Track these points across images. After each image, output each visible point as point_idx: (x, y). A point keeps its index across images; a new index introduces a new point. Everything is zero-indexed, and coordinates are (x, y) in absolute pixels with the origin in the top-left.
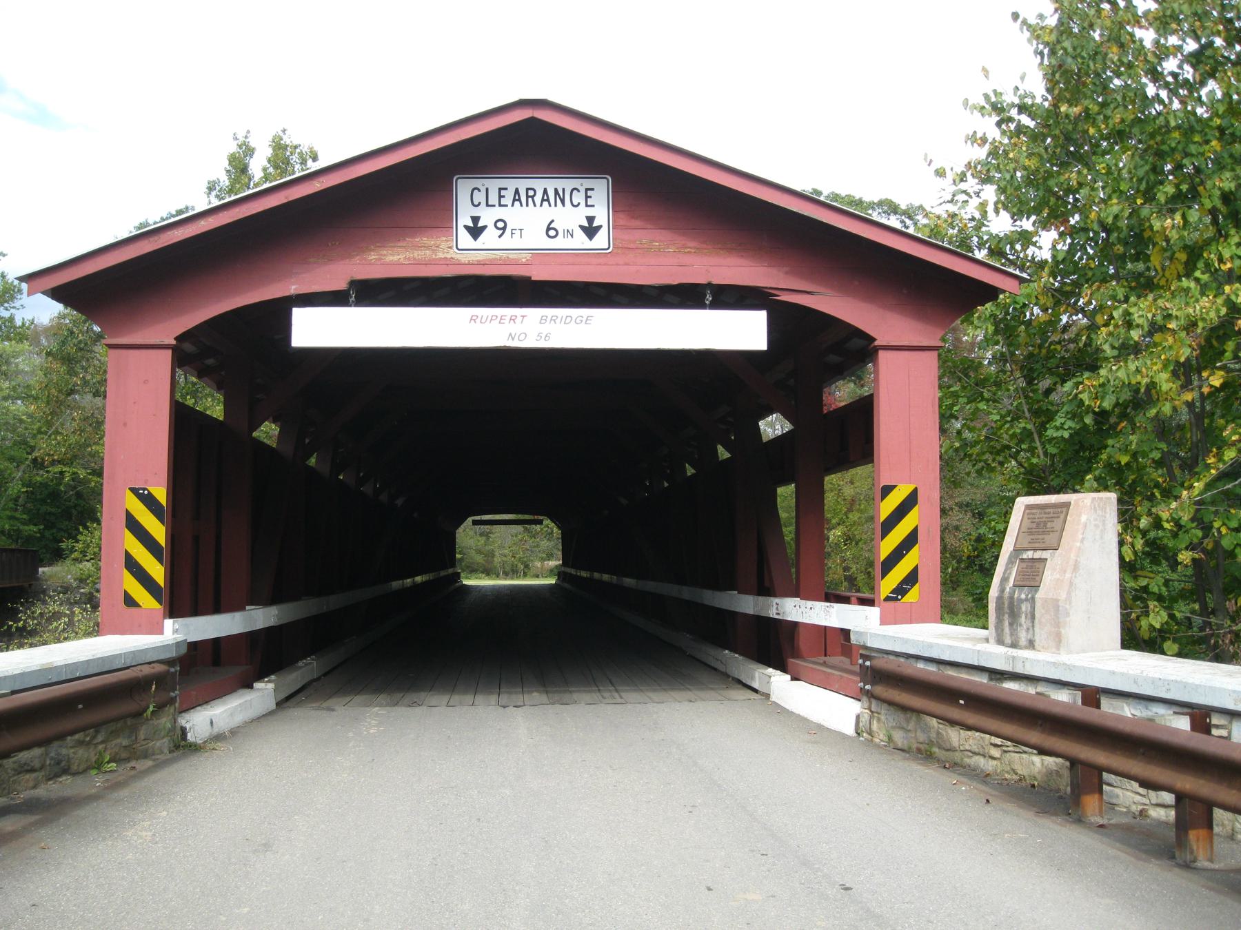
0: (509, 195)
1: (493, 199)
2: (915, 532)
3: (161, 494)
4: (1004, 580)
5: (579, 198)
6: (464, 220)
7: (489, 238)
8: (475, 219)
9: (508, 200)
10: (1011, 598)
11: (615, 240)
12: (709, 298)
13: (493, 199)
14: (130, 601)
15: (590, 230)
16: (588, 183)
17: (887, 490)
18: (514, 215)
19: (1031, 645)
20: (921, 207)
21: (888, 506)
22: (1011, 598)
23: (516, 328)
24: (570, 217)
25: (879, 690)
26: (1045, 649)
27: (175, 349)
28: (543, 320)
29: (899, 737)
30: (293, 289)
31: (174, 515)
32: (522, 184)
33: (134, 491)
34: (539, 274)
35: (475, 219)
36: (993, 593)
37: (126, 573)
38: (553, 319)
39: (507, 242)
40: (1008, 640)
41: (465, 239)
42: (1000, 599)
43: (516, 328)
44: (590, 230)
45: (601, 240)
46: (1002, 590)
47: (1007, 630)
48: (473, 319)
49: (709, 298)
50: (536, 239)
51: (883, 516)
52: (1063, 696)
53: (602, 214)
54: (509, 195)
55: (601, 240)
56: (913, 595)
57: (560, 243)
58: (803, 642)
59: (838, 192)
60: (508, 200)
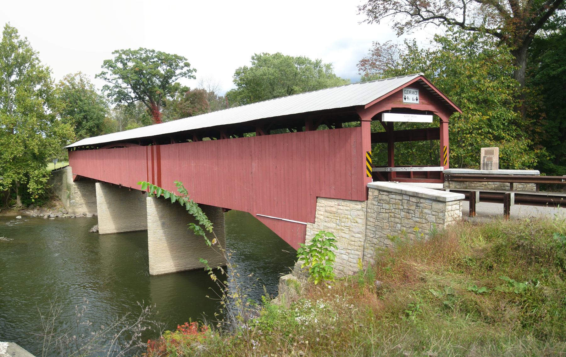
4: (484, 161)
6: (404, 97)
19: (491, 169)
20: (183, 57)
22: (487, 163)
25: (455, 179)
30: (385, 109)
34: (413, 108)
42: (484, 164)
44: (417, 100)
53: (418, 96)
55: (418, 102)
56: (446, 165)
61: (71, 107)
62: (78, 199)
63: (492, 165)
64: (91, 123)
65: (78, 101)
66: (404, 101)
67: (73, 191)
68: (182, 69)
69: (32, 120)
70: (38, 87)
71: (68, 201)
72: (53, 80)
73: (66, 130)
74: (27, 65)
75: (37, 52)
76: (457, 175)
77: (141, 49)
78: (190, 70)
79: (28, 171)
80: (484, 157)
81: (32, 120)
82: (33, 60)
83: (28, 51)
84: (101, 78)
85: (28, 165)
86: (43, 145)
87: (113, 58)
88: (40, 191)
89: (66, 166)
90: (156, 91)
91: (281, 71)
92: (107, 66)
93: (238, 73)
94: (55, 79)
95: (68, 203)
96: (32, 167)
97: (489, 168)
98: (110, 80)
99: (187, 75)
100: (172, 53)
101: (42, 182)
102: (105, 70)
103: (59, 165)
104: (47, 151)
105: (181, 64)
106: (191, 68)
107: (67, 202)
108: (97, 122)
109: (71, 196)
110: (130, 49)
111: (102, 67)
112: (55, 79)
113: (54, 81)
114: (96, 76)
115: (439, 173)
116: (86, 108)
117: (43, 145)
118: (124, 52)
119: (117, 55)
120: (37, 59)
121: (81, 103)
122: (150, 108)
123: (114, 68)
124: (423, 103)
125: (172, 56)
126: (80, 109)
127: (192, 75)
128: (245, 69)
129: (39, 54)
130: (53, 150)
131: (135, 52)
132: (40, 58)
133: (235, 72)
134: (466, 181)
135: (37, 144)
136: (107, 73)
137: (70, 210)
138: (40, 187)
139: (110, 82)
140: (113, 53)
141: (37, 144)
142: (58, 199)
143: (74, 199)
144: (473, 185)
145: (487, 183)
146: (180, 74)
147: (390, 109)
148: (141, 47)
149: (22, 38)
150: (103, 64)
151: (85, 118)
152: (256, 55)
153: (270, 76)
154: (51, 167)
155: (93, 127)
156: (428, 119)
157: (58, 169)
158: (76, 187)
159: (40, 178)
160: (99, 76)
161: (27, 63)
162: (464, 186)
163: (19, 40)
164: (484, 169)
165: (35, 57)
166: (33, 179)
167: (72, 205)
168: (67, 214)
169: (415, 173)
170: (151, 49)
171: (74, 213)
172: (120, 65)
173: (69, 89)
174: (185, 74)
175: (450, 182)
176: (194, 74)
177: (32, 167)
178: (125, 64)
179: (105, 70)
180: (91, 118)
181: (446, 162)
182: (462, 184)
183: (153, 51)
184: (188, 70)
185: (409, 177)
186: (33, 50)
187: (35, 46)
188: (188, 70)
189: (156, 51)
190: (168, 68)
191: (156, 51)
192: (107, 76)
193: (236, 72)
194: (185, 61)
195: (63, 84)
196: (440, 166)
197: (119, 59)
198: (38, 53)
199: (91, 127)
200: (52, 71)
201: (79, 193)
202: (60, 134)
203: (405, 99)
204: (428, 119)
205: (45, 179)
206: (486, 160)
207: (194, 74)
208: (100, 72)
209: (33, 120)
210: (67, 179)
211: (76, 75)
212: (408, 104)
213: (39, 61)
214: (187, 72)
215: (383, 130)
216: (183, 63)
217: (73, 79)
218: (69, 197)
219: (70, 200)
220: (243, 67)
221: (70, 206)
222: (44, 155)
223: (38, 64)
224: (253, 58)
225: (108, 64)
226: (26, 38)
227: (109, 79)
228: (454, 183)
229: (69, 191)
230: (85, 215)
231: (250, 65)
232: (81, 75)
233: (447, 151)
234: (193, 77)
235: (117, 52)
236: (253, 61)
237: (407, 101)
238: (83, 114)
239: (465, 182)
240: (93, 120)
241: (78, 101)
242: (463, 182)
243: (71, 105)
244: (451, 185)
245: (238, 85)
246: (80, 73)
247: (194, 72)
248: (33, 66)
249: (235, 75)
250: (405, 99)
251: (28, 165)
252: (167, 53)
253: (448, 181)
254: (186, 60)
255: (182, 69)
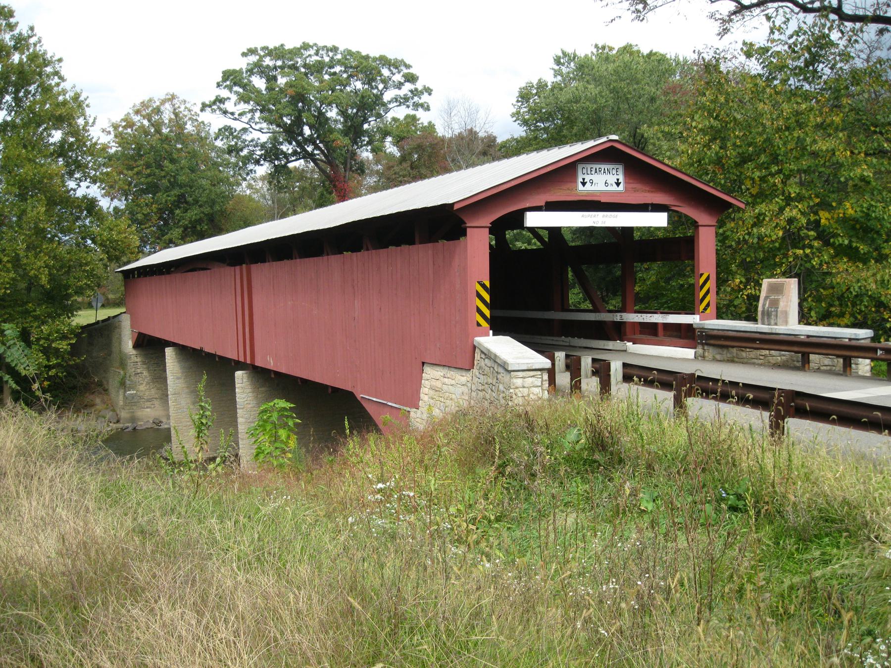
0: (594, 170)
1: (589, 172)
2: (709, 289)
3: (487, 284)
4: (764, 305)
5: (614, 172)
6: (580, 180)
7: (588, 187)
8: (584, 179)
9: (593, 172)
10: (768, 310)
11: (626, 188)
12: (650, 208)
13: (589, 172)
14: (479, 325)
15: (618, 184)
16: (617, 166)
17: (702, 275)
18: (596, 178)
19: (776, 324)
20: (402, 61)
21: (702, 281)
22: (768, 310)
23: (595, 219)
24: (612, 179)
25: (712, 342)
26: (782, 325)
27: (490, 228)
28: (603, 216)
29: (718, 357)
30: (528, 205)
31: (491, 291)
32: (598, 166)
33: (479, 282)
34: (603, 200)
35: (584, 179)
36: (760, 309)
37: (477, 314)
38: (607, 216)
39: (593, 188)
40: (766, 323)
41: (580, 187)
42: (763, 312)
43: (595, 219)
44: (618, 184)
45: (621, 188)
46: (764, 308)
47: (766, 320)
48: (583, 216)
49: (650, 208)
50: (601, 187)
51: (701, 284)
52: (803, 337)
53: (621, 178)
54: (594, 170)
55: (621, 188)
56: (708, 311)
57: (609, 188)
58: (628, 330)
59: (350, 48)
60: (593, 172)
61: (149, 175)
62: (142, 388)
63: (777, 316)
64: (193, 213)
65: (166, 163)
66: (580, 187)
67: (131, 370)
68: (400, 89)
69: (35, 213)
70: (57, 136)
71: (121, 392)
72: (91, 121)
73: (119, 233)
74: (32, 88)
75: (56, 58)
76: (715, 333)
77: (306, 46)
78: (416, 89)
79: (26, 325)
80: (766, 298)
81: (35, 213)
82: (48, 76)
83: (34, 57)
84: (213, 111)
85: (27, 312)
86: (61, 267)
87: (241, 64)
88: (52, 372)
89: (121, 313)
90: (333, 141)
91: (614, 91)
92: (228, 83)
93: (524, 96)
94: (95, 119)
95: (121, 397)
96: (36, 318)
97: (773, 322)
98: (236, 116)
99: (410, 103)
100: (374, 53)
101: (57, 350)
102: (224, 93)
103: (104, 314)
104: (72, 281)
105: (398, 78)
106: (419, 85)
107: (118, 396)
108: (207, 210)
109: (128, 382)
110: (282, 45)
111: (219, 85)
112: (95, 119)
113: (94, 123)
114: (204, 106)
115: (690, 326)
116: (182, 178)
117: (61, 267)
118: (270, 53)
119: (253, 59)
120: (56, 73)
121: (171, 166)
122: (328, 176)
123: (244, 87)
124: (635, 190)
125: (375, 59)
126: (169, 181)
127: (421, 101)
128: (541, 86)
129: (61, 64)
130: (87, 277)
131: (296, 52)
132: (62, 73)
133: (518, 95)
134: (733, 347)
135: (47, 266)
136: (229, 98)
137: (124, 414)
138: (54, 361)
139: (235, 119)
140: (244, 55)
141: (47, 266)
142: (102, 388)
143: (134, 389)
144: (744, 354)
145: (767, 352)
146: (395, 99)
147: (543, 204)
148: (307, 41)
149: (22, 29)
150: (220, 79)
151: (181, 199)
152: (564, 53)
153: (588, 103)
154: (84, 318)
155: (200, 221)
156: (659, 220)
157: (103, 321)
158: (139, 359)
159: (53, 341)
160: (210, 106)
161: (34, 83)
162: (729, 355)
163: (16, 32)
164: (763, 324)
165: (51, 70)
166: (38, 344)
167: (132, 402)
168: (118, 421)
169: (667, 326)
170: (329, 45)
171: (133, 419)
172: (259, 83)
173: (147, 133)
174: (406, 99)
175: (706, 347)
176: (425, 98)
177: (36, 318)
178: (271, 79)
179: (224, 93)
180: (196, 201)
181: (708, 305)
182: (725, 352)
183: (335, 49)
184: (411, 91)
185: (655, 334)
186: (48, 56)
187: (50, 47)
188: (411, 91)
189: (341, 49)
190: (366, 86)
191: (341, 49)
192: (229, 106)
193: (521, 92)
194: (405, 71)
195: (130, 124)
196: (694, 314)
197: (258, 68)
198: (60, 60)
199: (196, 221)
200: (87, 102)
201: (145, 373)
202: (103, 241)
203: (584, 184)
204: (659, 220)
205: (65, 343)
206: (767, 306)
207: (425, 98)
208: (213, 98)
209: (37, 209)
210: (120, 344)
211: (163, 102)
212: (593, 193)
213: (62, 78)
214: (410, 94)
215: (614, 240)
216: (402, 73)
217: (158, 111)
218: (123, 384)
219: (125, 392)
220: (535, 82)
221: (125, 404)
222: (67, 290)
223: (58, 85)
224: (558, 61)
225: (231, 78)
226: (32, 29)
227: (232, 114)
228: (711, 349)
229: (124, 369)
230: (157, 424)
231: (550, 79)
232: (175, 101)
233: (711, 285)
234: (422, 105)
235: (252, 51)
236: (557, 68)
237: (588, 187)
238: (176, 192)
239: (730, 349)
240: (200, 206)
241: (166, 163)
242: (727, 347)
243: (148, 171)
244: (706, 354)
245: (525, 123)
246: (173, 97)
247: (426, 94)
248: (46, 90)
249: (518, 101)
250: (584, 184)
251: (27, 312)
252: (364, 54)
253: (703, 344)
254: (408, 66)
255: (400, 89)
